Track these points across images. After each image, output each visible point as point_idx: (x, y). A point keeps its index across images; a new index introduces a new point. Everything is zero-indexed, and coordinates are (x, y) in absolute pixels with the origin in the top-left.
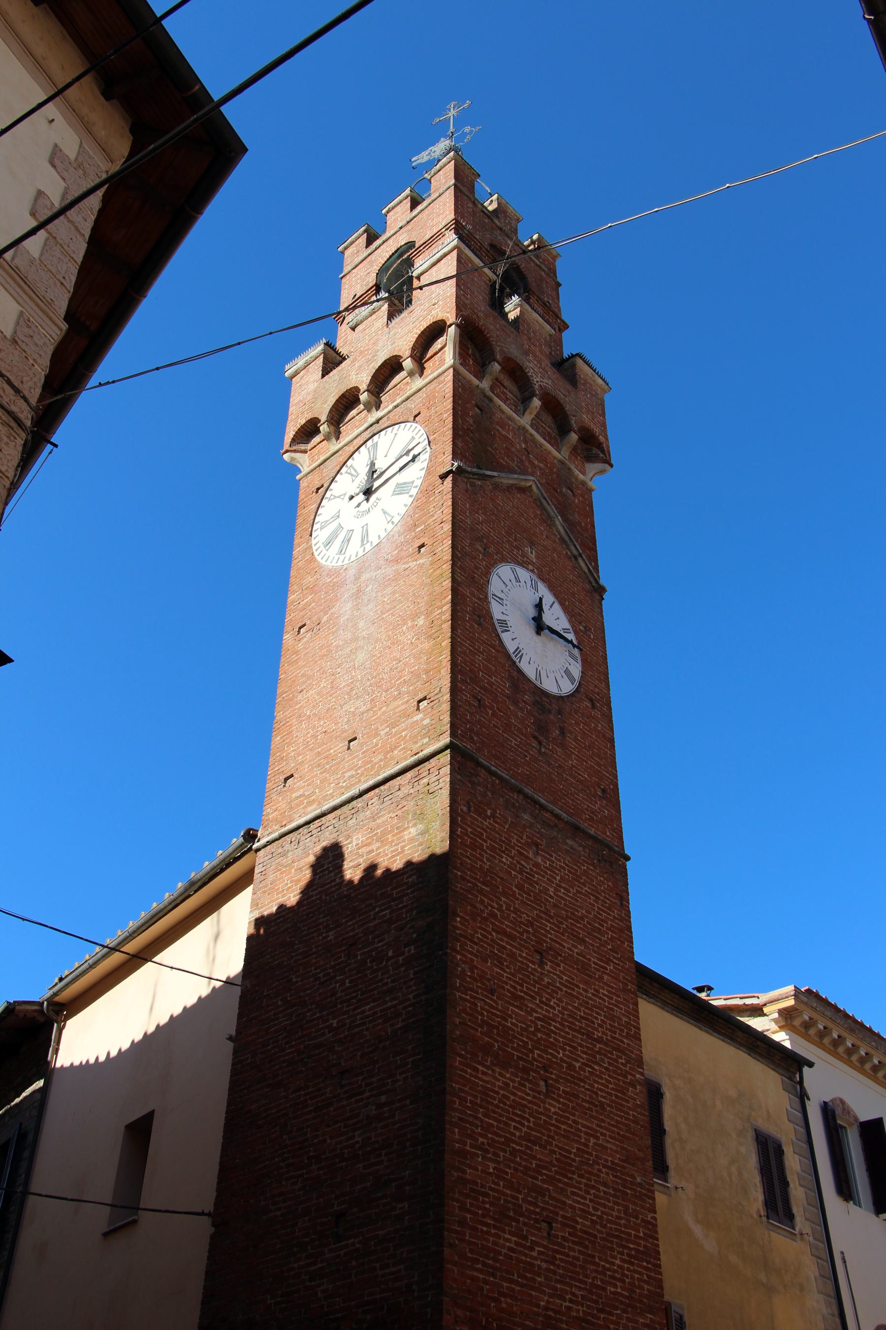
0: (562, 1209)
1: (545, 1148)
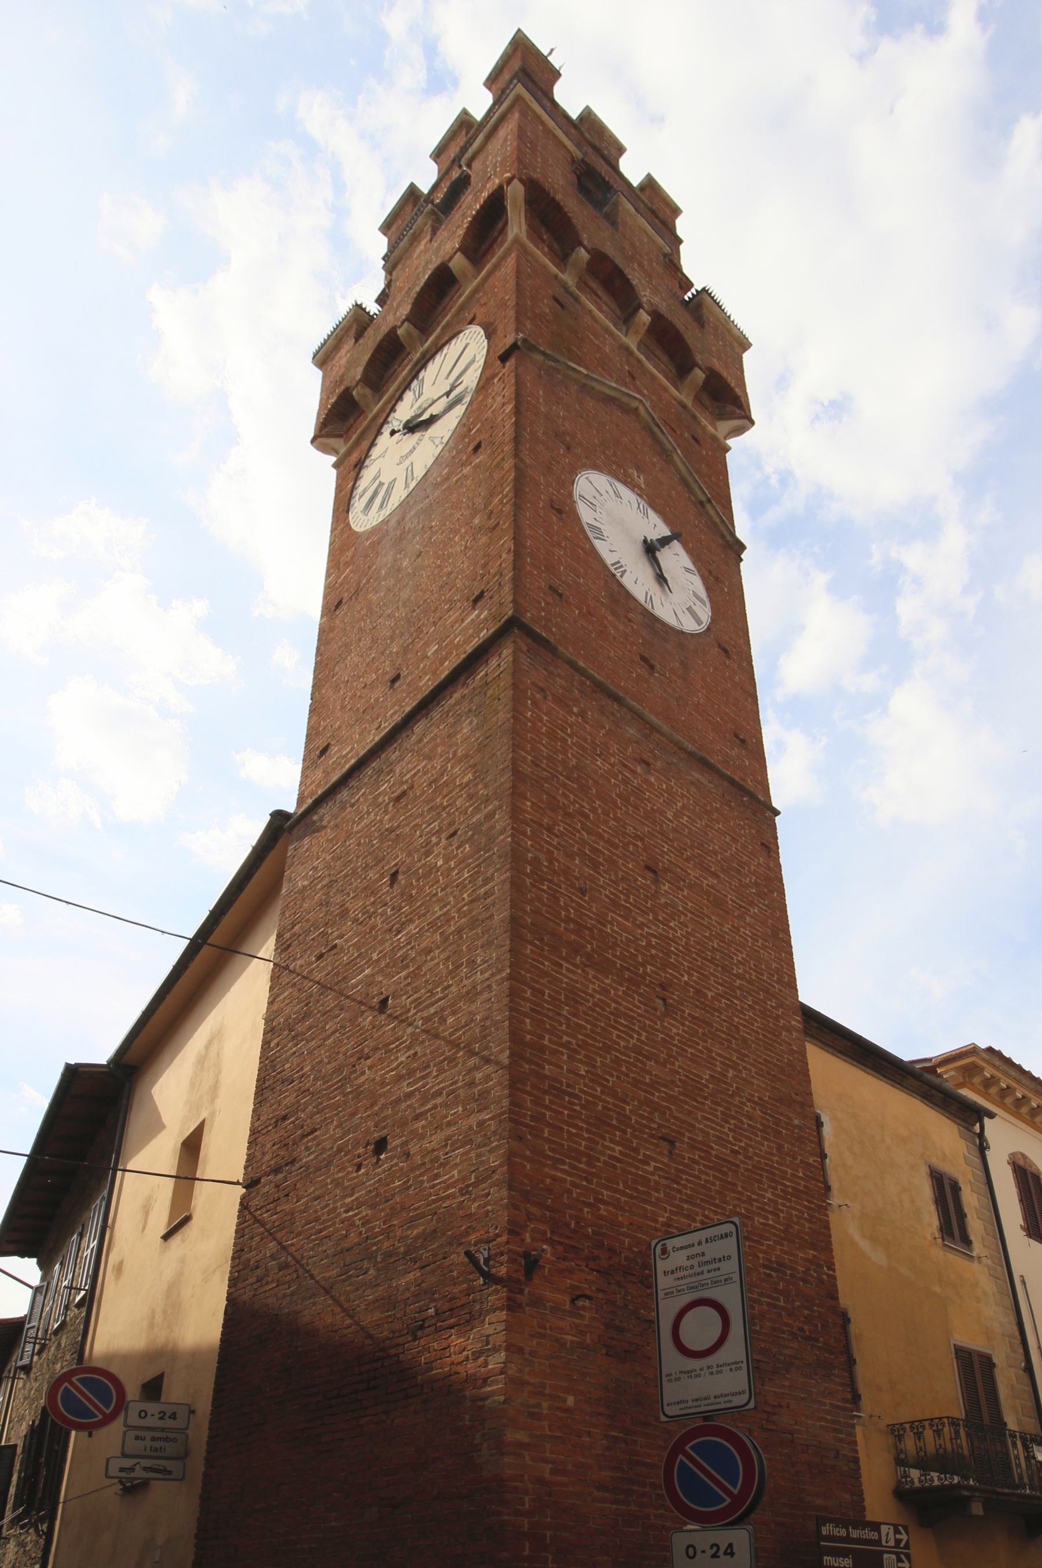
0: (690, 1131)
1: (664, 1065)
